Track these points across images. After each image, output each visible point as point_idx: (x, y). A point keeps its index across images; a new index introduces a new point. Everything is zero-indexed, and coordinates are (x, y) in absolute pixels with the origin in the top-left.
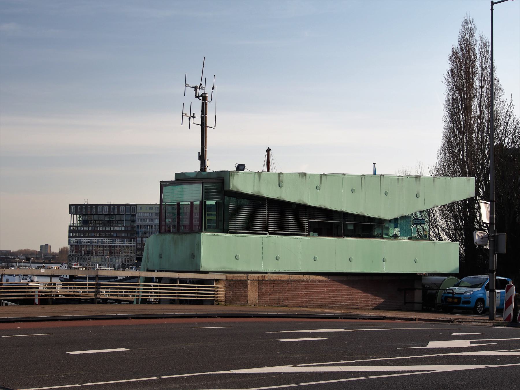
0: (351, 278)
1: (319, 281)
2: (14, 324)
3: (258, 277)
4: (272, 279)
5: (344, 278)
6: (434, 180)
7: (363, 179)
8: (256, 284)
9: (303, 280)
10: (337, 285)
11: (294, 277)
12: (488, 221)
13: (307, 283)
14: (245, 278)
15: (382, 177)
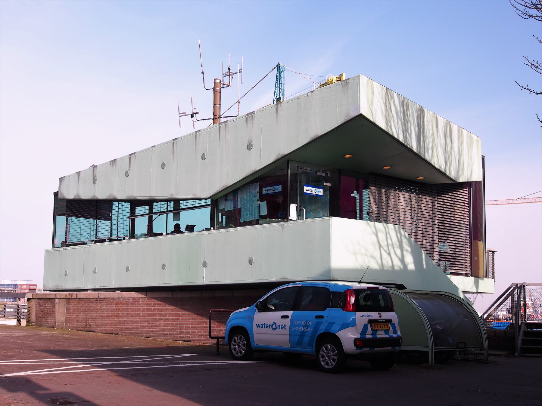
0: (194, 295)
1: (134, 299)
2: (526, 293)
3: (66, 295)
4: (79, 297)
5: (169, 295)
6: (277, 108)
7: (175, 144)
8: (64, 303)
9: (114, 299)
10: (158, 305)
11: (81, 294)
12: (383, 305)
13: (118, 303)
14: (53, 297)
15: (198, 133)
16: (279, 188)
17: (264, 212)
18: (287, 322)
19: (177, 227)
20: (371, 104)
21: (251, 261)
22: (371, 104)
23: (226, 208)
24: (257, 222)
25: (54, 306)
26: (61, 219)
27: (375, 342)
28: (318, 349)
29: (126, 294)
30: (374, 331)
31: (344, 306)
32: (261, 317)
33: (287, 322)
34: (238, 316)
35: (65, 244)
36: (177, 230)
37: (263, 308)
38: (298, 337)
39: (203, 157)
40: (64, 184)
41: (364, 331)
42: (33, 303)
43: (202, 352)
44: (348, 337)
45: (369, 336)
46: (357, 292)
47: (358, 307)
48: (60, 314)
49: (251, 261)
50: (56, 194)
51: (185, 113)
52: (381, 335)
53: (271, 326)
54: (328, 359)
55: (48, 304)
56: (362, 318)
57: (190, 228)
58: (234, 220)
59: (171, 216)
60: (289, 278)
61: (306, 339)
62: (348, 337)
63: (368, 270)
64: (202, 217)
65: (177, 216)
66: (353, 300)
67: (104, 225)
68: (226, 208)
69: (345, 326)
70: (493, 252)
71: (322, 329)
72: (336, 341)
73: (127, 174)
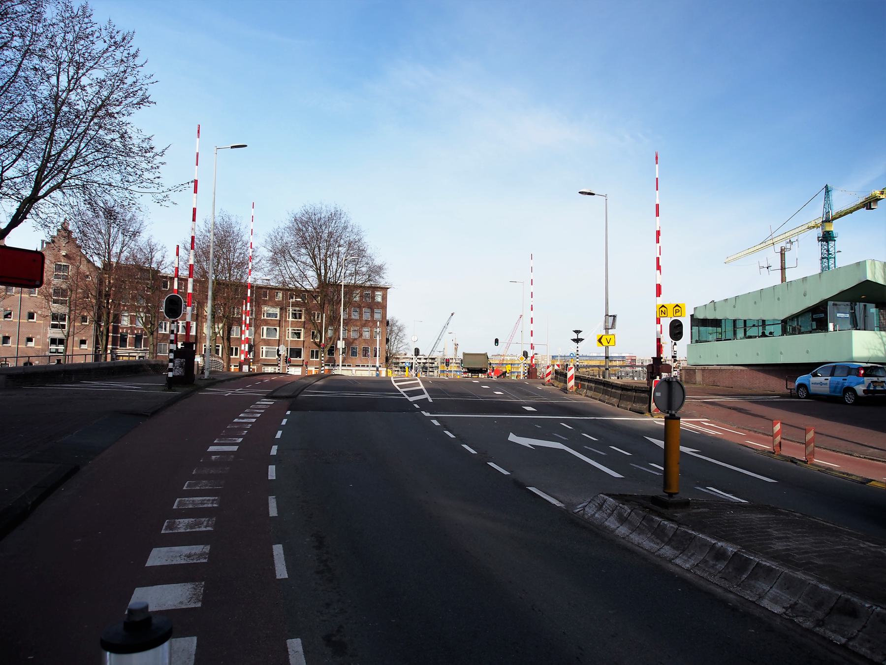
13: (732, 371)
16: (822, 315)
17: (815, 327)
18: (828, 382)
19: (763, 333)
20: (874, 274)
21: (808, 352)
22: (874, 274)
23: (790, 325)
24: (810, 332)
25: (695, 373)
26: (695, 329)
27: (875, 391)
28: (844, 394)
29: (736, 367)
30: (875, 387)
31: (858, 375)
32: (814, 380)
33: (828, 382)
34: (800, 379)
35: (697, 342)
36: (764, 335)
37: (815, 375)
38: (833, 388)
39: (779, 299)
40: (697, 311)
41: (869, 386)
42: (683, 372)
43: (783, 396)
44: (860, 389)
45: (871, 389)
46: (865, 368)
47: (865, 375)
48: (699, 377)
49: (808, 352)
50: (692, 316)
51: (613, 327)
52: (879, 388)
53: (819, 383)
54: (849, 398)
55: (692, 372)
56: (867, 380)
57: (771, 333)
58: (796, 331)
59: (761, 328)
60: (829, 360)
61: (838, 390)
62: (860, 389)
63: (878, 357)
64: (778, 329)
65: (764, 328)
66: (862, 372)
67: (719, 329)
68: (790, 325)
69: (858, 384)
70: (614, 317)
71: (846, 385)
72: (854, 391)
73: (734, 307)
